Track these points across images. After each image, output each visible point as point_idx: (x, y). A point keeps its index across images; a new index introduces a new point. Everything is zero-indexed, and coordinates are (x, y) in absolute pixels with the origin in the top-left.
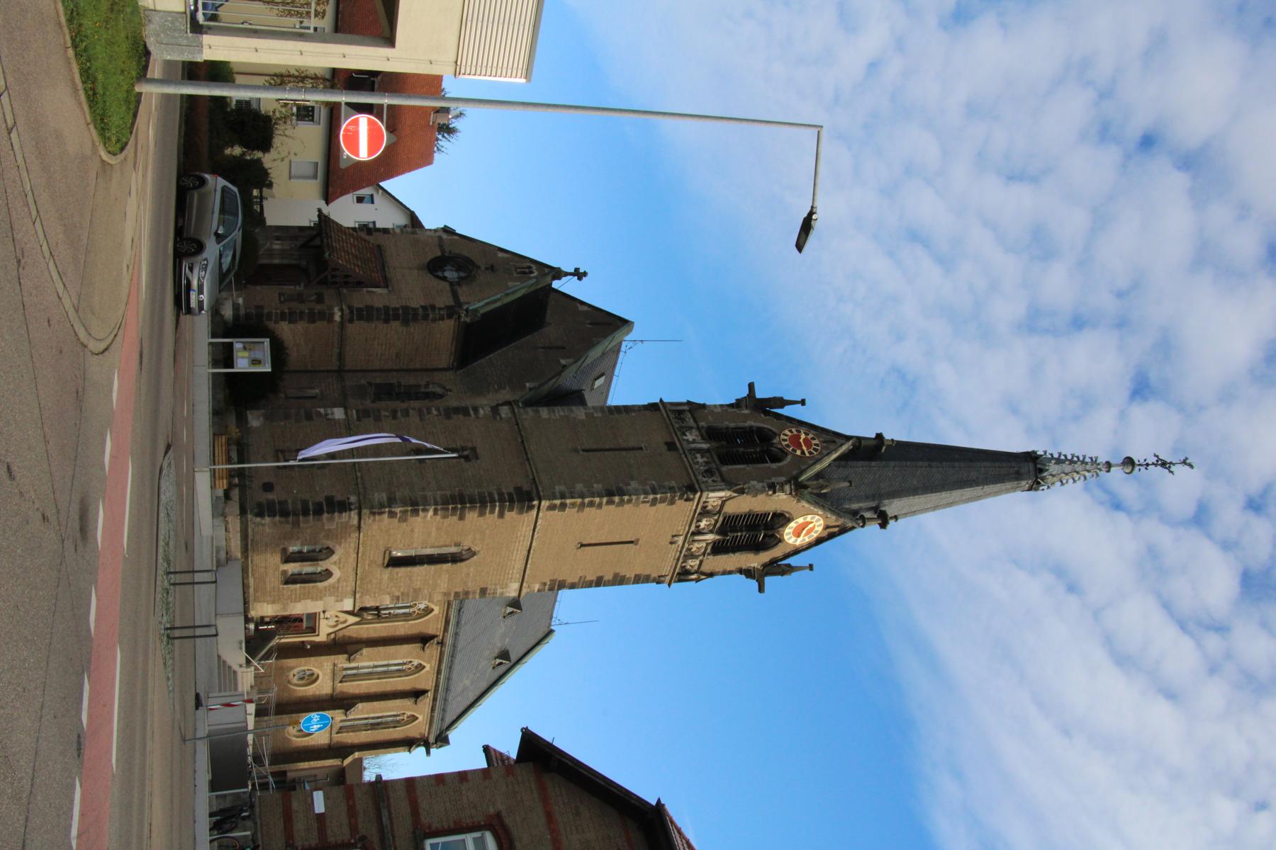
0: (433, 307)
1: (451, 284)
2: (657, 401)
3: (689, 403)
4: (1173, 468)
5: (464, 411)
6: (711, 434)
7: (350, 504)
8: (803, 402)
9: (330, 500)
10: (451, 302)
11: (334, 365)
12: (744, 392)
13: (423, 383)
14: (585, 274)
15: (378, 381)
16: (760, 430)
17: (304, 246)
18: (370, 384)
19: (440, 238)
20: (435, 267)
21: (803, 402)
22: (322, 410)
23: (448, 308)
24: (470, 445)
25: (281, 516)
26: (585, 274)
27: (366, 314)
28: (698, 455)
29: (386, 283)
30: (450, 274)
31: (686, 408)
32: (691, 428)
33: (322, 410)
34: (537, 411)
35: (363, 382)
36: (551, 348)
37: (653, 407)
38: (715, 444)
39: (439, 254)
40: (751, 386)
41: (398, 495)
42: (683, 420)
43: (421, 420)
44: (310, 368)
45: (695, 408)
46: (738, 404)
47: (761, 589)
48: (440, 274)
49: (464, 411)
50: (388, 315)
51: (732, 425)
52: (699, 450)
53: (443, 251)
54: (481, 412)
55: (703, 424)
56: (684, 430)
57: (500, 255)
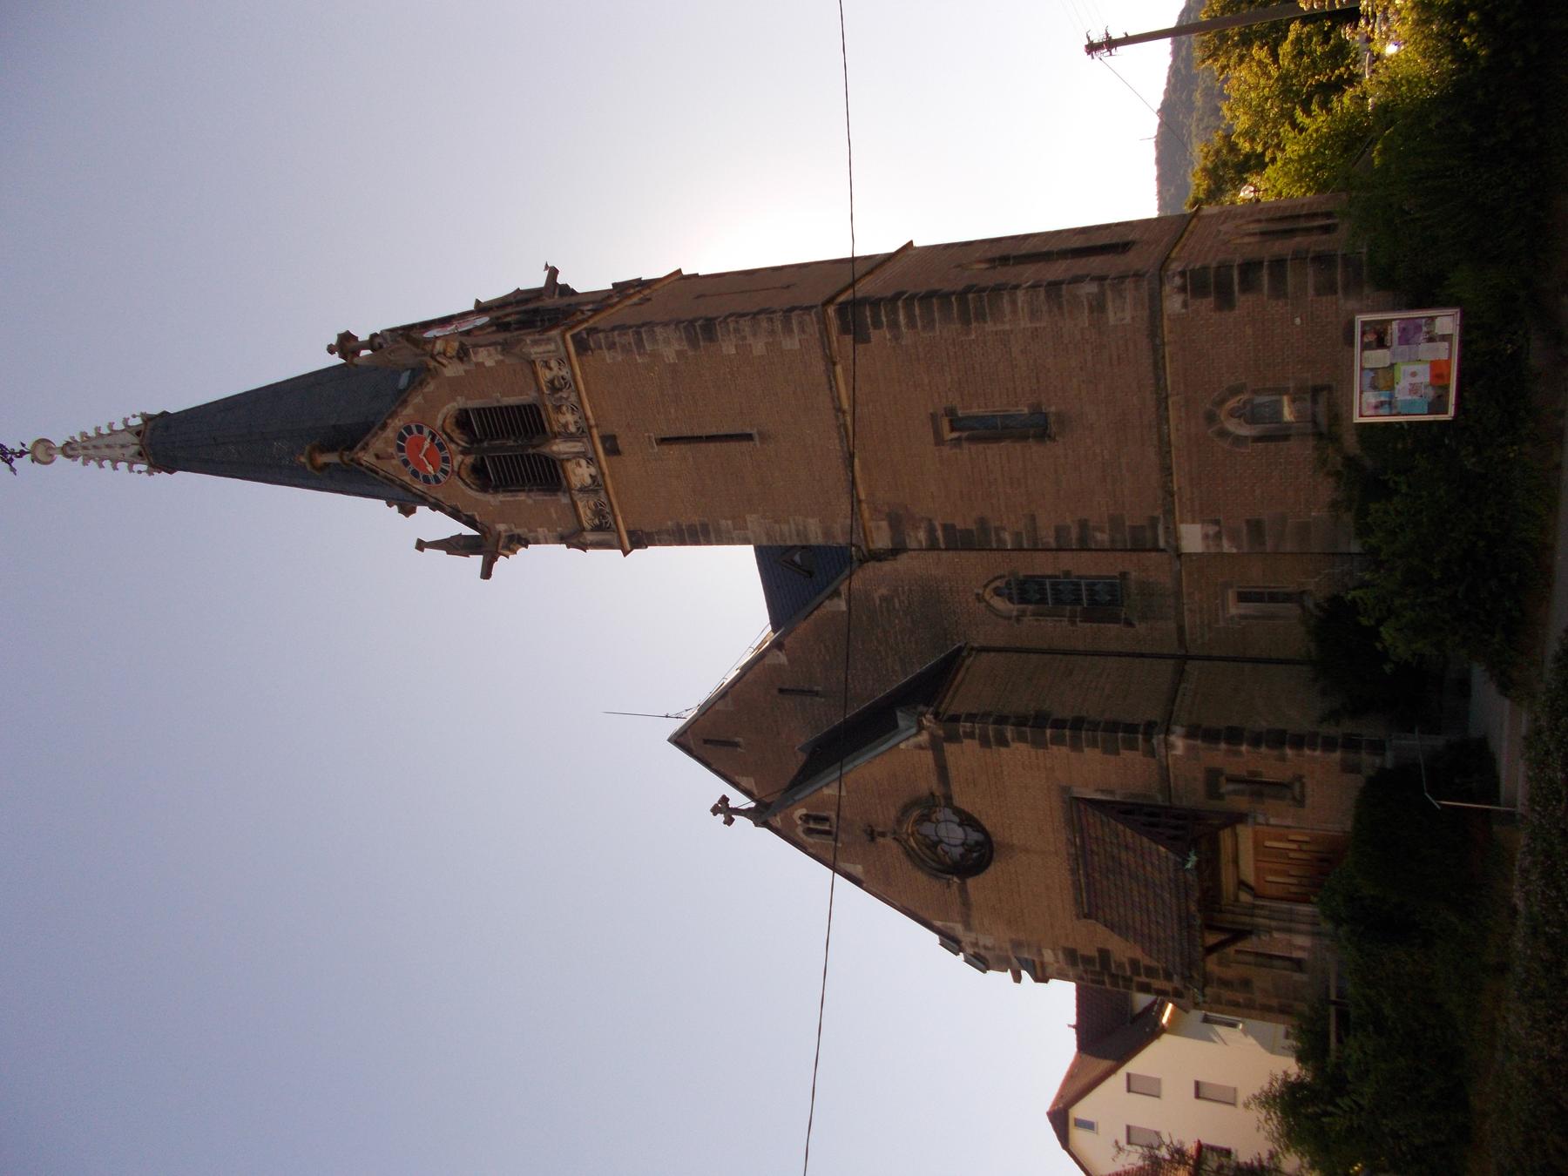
0: (985, 742)
1: (948, 798)
2: (539, 281)
3: (584, 547)
4: (17, 462)
5: (959, 540)
6: (549, 476)
7: (1183, 289)
8: (421, 545)
9: (1225, 300)
10: (950, 749)
11: (1190, 666)
12: (501, 564)
13: (1028, 620)
14: (715, 811)
15: (1113, 628)
16: (484, 488)
17: (1239, 934)
18: (1129, 624)
19: (968, 926)
20: (979, 856)
21: (421, 545)
22: (1227, 547)
23: (953, 738)
24: (947, 451)
25: (1228, 742)
26: (715, 811)
27: (1119, 732)
28: (572, 429)
29: (1078, 809)
30: (954, 835)
31: (590, 537)
32: (583, 490)
33: (1227, 547)
34: (827, 533)
35: (1141, 628)
36: (802, 692)
37: (639, 540)
38: (545, 450)
39: (970, 882)
40: (486, 573)
41: (1084, 319)
42: (598, 513)
43: (1033, 518)
44: (1248, 667)
45: (574, 538)
46: (517, 541)
47: (553, 272)
48: (975, 836)
49: (959, 540)
50: (1074, 729)
51: (522, 497)
52: (570, 437)
53: (963, 890)
54: (922, 535)
55: (565, 500)
56: (596, 486)
57: (858, 870)
